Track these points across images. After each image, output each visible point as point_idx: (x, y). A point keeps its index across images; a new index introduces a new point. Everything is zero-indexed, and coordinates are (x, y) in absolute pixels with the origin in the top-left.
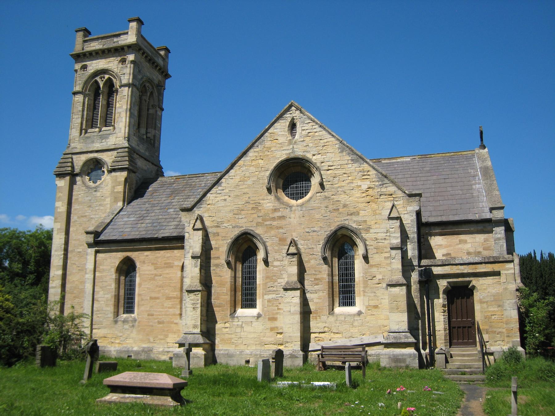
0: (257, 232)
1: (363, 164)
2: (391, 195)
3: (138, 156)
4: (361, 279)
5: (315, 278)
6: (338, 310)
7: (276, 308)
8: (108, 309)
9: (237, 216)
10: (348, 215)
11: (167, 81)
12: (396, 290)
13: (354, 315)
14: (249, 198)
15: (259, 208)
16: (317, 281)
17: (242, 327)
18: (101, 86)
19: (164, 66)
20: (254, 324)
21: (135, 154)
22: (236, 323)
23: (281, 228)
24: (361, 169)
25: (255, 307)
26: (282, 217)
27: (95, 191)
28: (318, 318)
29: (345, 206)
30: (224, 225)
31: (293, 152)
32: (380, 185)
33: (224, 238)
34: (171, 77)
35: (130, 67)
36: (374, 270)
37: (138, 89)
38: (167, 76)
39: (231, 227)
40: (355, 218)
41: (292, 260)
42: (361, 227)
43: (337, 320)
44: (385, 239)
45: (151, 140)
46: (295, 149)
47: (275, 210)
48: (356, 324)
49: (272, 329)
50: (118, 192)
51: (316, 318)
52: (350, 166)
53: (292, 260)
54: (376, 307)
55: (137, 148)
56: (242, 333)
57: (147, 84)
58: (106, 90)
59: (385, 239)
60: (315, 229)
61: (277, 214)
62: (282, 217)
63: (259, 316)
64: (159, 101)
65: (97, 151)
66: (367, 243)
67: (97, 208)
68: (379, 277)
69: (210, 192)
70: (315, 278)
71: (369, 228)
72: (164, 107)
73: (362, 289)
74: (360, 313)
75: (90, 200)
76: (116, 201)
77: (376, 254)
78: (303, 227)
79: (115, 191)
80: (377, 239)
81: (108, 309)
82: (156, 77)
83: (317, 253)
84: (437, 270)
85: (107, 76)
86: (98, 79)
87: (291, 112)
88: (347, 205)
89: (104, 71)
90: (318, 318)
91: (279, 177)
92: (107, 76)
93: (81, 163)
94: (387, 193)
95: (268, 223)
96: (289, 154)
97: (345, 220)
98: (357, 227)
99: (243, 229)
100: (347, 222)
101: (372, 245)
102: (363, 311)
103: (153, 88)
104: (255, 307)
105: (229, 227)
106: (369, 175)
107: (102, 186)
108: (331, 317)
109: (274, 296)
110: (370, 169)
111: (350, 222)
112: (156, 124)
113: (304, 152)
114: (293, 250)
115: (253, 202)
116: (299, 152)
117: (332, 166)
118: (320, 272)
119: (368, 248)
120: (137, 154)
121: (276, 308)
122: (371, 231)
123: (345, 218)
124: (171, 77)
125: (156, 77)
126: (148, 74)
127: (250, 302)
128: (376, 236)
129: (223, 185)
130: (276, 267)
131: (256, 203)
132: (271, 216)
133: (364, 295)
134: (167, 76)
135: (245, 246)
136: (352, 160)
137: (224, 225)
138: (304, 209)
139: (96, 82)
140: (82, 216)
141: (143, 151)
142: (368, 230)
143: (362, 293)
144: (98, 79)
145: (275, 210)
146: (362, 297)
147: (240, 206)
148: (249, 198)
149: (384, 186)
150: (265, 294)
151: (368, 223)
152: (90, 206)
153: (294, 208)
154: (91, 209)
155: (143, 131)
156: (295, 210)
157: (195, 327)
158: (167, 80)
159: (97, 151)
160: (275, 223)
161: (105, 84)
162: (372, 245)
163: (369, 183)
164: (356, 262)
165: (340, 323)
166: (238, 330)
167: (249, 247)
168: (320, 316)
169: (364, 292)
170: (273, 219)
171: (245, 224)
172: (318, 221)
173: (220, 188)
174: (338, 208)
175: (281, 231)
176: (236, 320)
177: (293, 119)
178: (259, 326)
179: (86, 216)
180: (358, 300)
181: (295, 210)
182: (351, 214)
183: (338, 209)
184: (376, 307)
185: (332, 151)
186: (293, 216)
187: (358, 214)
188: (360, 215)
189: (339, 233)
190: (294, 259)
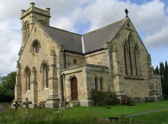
11: (50, 19)
23: (33, 64)
38: (49, 17)
85: (27, 23)
189: (44, 63)
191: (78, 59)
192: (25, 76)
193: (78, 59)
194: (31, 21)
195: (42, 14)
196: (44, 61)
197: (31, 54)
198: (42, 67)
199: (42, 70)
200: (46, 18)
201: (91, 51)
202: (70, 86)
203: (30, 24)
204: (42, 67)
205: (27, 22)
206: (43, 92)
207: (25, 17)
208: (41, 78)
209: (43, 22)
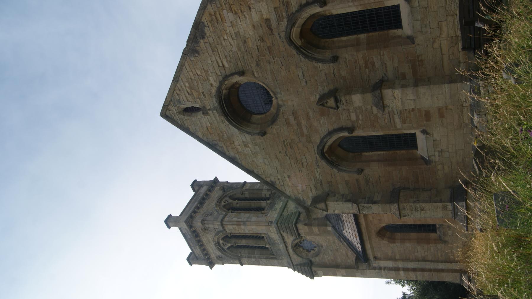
0: (318, 141)
1: (203, 23)
3: (285, 210)
6: (407, 29)
7: (412, 113)
8: (432, 248)
9: (305, 164)
10: (273, 34)
14: (280, 152)
15: (290, 141)
17: (441, 151)
18: (229, 245)
20: (436, 136)
22: (437, 158)
23: (307, 115)
24: (210, 25)
25: (415, 134)
27: (322, 247)
28: (420, 58)
29: (262, 39)
31: (215, 109)
33: (333, 176)
34: (216, 177)
35: (208, 224)
37: (225, 216)
39: (318, 170)
40: (274, 24)
41: (344, 102)
42: (284, 14)
43: (421, 32)
45: (271, 193)
46: (212, 107)
47: (288, 123)
49: (442, 116)
50: (319, 231)
51: (422, 60)
52: (210, 39)
53: (344, 102)
55: (278, 210)
57: (223, 203)
58: (233, 241)
60: (300, 74)
62: (294, 113)
63: (424, 132)
64: (237, 188)
65: (286, 247)
67: (337, 245)
70: (366, 68)
72: (243, 182)
75: (331, 250)
79: (318, 233)
81: (432, 248)
85: (221, 242)
86: (226, 248)
89: (218, 244)
90: (420, 58)
91: (249, 121)
92: (221, 242)
93: (299, 258)
95: (305, 130)
96: (218, 113)
97: (280, 37)
100: (283, 35)
103: (226, 196)
105: (319, 171)
107: (316, 242)
108: (417, 41)
110: (206, 13)
111: (282, 29)
112: (258, 190)
113: (212, 97)
114: (331, 102)
117: (217, 62)
118: (356, 62)
120: (283, 211)
121: (412, 113)
123: (278, 38)
124: (216, 177)
127: (410, 141)
129: (273, 180)
130: (357, 117)
131: (285, 145)
136: (203, 37)
139: (228, 248)
140: (347, 256)
144: (226, 248)
145: (288, 123)
148: (280, 152)
150: (395, 127)
152: (337, 250)
155: (263, 204)
156: (282, 100)
157: (445, 208)
158: (220, 181)
159: (286, 247)
160: (304, 122)
161: (228, 242)
163: (225, 12)
164: (335, 12)
165: (426, 27)
167: (339, 145)
168: (418, 57)
170: (299, 124)
171: (311, 156)
172: (289, 71)
173: (277, 182)
174: (266, 47)
176: (433, 158)
177: (179, 112)
178: (438, 133)
179: (346, 253)
182: (271, 29)
183: (268, 47)
185: (200, 63)
186: (290, 103)
187: (267, 20)
188: (268, 17)
189: (299, 43)
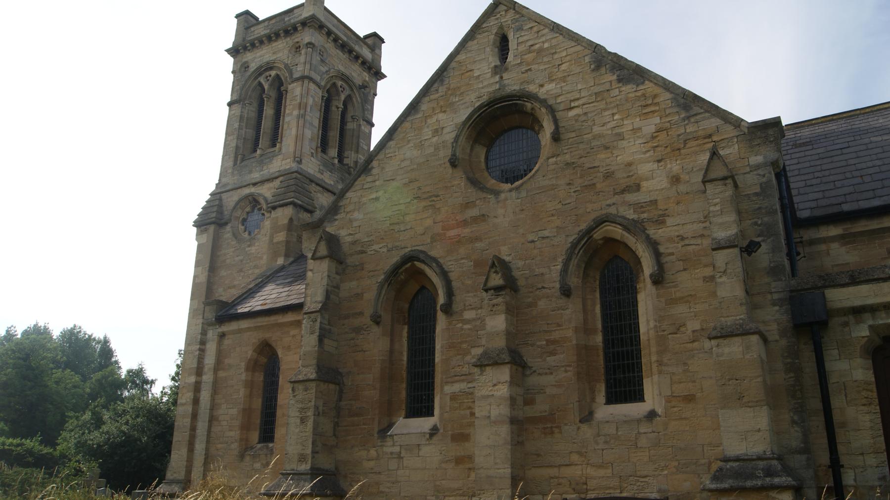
1: (643, 83)
2: (710, 136)
4: (652, 332)
5: (547, 341)
6: (605, 412)
8: (232, 434)
11: (380, 84)
12: (733, 349)
13: (639, 421)
14: (419, 188)
15: (437, 206)
16: (552, 347)
17: (400, 457)
18: (266, 87)
19: (373, 60)
20: (426, 450)
21: (314, 185)
23: (478, 239)
25: (433, 415)
26: (483, 218)
28: (556, 430)
29: (608, 175)
30: (374, 247)
31: (502, 87)
32: (684, 120)
33: (371, 274)
34: (385, 76)
36: (680, 310)
38: (380, 76)
39: (385, 250)
40: (631, 197)
41: (495, 301)
42: (645, 215)
43: (598, 435)
44: (702, 236)
45: (350, 167)
47: (467, 205)
48: (643, 442)
49: (459, 461)
50: (278, 243)
51: (552, 433)
52: (616, 92)
53: (495, 301)
54: (689, 399)
55: (319, 175)
56: (400, 472)
57: (340, 83)
58: (273, 94)
59: (702, 236)
60: (546, 233)
61: (474, 212)
62: (483, 218)
63: (434, 431)
64: (364, 110)
65: (254, 184)
66: (662, 249)
67: (250, 272)
68: (694, 325)
69: (353, 189)
70: (547, 341)
71: (664, 215)
72: (374, 121)
73: (654, 358)
74: (652, 415)
76: (274, 256)
77: (683, 273)
78: (521, 231)
79: (275, 241)
80: (683, 238)
82: (358, 75)
83: (551, 285)
84: (842, 297)
85: (273, 73)
86: (262, 80)
87: (498, 16)
88: (613, 173)
89: (269, 67)
90: (556, 430)
92: (273, 73)
94: (701, 133)
97: (609, 205)
98: (635, 217)
99: (407, 250)
101: (672, 254)
102: (659, 411)
104: (433, 415)
106: (657, 104)
108: (584, 427)
109: (463, 386)
110: (658, 90)
113: (521, 84)
115: (425, 196)
116: (513, 82)
117: (578, 99)
118: (559, 325)
119: (664, 260)
120: (317, 184)
121: (468, 412)
122: (670, 221)
123: (608, 202)
124: (385, 76)
125: (358, 75)
126: (342, 68)
128: (681, 232)
129: (374, 171)
130: (468, 322)
131: (431, 197)
132: (460, 217)
133: (660, 372)
134: (380, 76)
135: (413, 287)
137: (374, 247)
138: (523, 194)
139: (260, 84)
140: (229, 288)
141: (332, 183)
142: (660, 221)
143: (654, 366)
144: (262, 80)
146: (656, 377)
147: (402, 207)
148: (419, 188)
149: (692, 120)
150: (447, 383)
151: (661, 206)
152: (241, 271)
153: (503, 196)
154: (242, 274)
155: (333, 152)
156: (506, 199)
157: (302, 458)
158: (379, 82)
161: (271, 85)
162: (672, 254)
163: (657, 120)
165: (606, 442)
166: (393, 464)
168: (559, 427)
169: (660, 363)
172: (553, 215)
173: (369, 179)
174: (594, 181)
175: (478, 245)
178: (432, 453)
179: (234, 287)
180: (649, 387)
181: (506, 199)
182: (623, 192)
183: (594, 184)
184: (689, 399)
187: (638, 188)
188: (643, 189)
189: (598, 235)
190: (500, 300)
191: (763, 241)
192: (386, 318)
193: (763, 241)
194: (300, 68)
195: (350, 51)
196: (600, 222)
197: (459, 180)
198: (574, 262)
199: (574, 281)
200: (366, 76)
201: (846, 208)
202: (875, 395)
203: (297, 79)
204: (574, 262)
205: (271, 68)
206: (587, 431)
207: (261, 42)
208: (570, 333)
209: (352, 90)
